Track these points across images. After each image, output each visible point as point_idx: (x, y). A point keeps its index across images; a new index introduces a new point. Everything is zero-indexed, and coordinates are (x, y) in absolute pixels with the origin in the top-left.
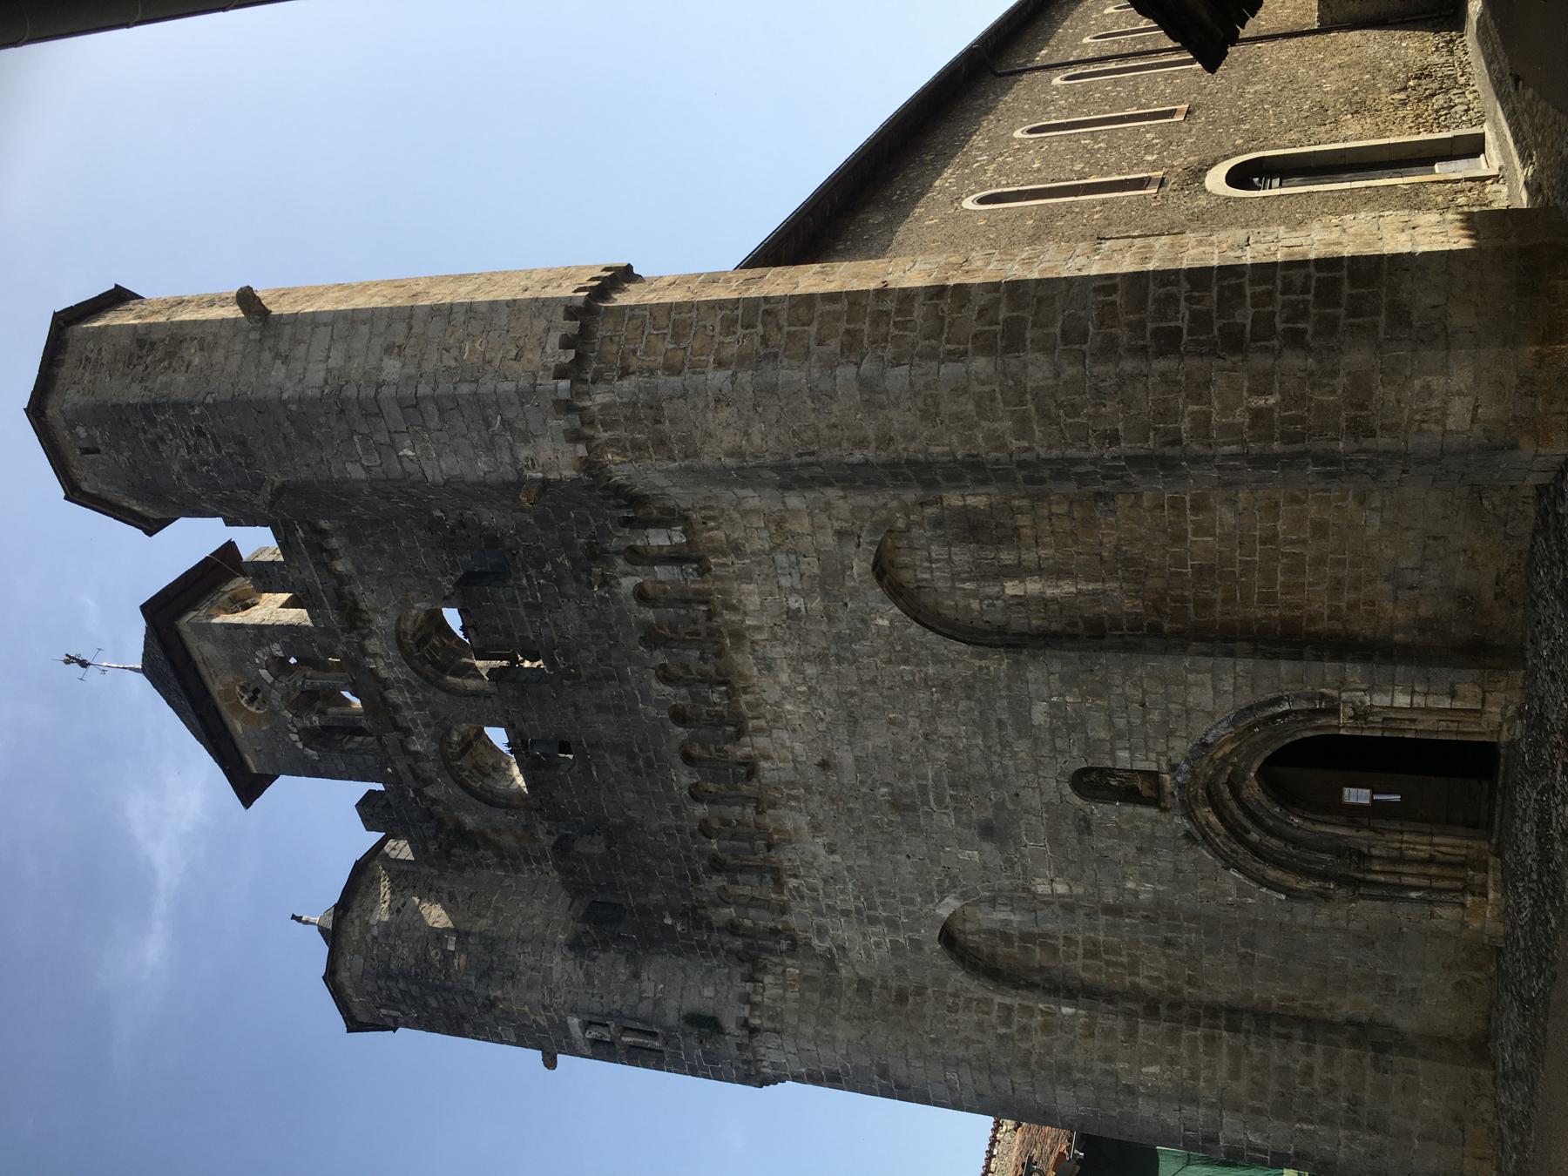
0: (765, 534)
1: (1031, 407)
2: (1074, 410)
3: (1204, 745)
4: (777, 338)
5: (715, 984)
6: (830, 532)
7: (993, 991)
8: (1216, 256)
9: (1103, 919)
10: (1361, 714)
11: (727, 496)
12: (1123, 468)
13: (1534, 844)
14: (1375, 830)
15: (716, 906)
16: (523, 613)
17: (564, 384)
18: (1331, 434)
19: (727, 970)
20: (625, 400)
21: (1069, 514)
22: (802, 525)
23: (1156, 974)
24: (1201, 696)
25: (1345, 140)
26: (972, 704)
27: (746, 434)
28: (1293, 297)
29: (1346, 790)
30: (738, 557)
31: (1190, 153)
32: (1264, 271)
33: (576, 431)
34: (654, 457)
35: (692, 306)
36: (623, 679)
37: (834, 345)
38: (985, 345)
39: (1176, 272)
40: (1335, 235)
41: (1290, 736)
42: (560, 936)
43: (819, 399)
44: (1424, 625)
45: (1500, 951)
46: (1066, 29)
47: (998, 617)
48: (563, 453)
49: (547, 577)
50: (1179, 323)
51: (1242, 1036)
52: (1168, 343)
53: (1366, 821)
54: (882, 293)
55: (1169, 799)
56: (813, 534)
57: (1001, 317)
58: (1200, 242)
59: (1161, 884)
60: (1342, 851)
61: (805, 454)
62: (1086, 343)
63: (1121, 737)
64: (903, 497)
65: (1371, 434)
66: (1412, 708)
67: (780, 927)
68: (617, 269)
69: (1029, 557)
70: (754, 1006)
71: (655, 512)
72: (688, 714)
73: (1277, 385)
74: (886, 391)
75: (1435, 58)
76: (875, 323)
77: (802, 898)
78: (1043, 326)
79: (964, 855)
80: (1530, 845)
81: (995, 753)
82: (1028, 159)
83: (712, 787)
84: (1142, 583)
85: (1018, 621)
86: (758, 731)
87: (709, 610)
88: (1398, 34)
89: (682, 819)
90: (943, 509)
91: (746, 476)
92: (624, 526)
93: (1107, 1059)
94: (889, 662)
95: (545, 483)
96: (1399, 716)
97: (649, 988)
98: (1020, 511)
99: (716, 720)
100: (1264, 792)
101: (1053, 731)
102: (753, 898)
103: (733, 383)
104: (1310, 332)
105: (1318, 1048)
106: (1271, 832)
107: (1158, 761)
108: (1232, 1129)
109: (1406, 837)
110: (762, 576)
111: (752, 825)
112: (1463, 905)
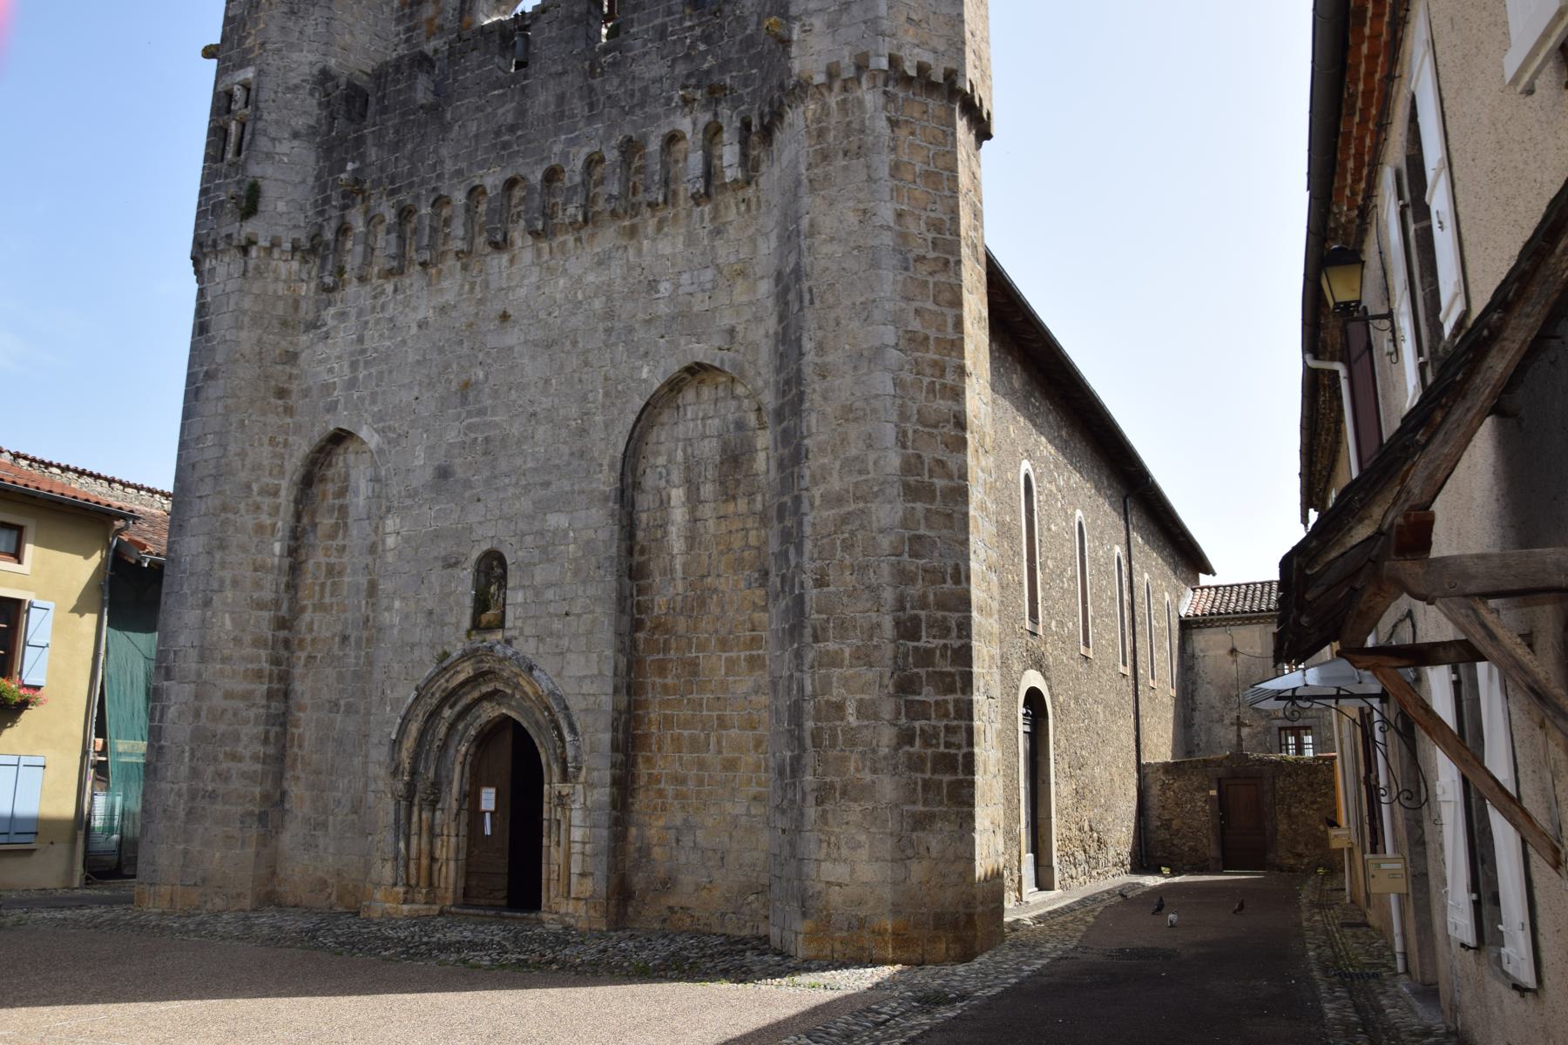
0: (732, 259)
1: (852, 507)
2: (848, 546)
3: (531, 669)
4: (923, 269)
5: (289, 213)
6: (733, 322)
7: (291, 479)
8: (980, 670)
9: (363, 581)
10: (562, 801)
11: (770, 222)
12: (792, 590)
13: (454, 939)
14: (458, 814)
15: (366, 212)
16: (658, 21)
17: (884, 63)
18: (820, 770)
19: (302, 224)
20: (867, 123)
21: (747, 546)
22: (740, 293)
23: (316, 627)
24: (577, 665)
25: (1056, 783)
26: (566, 458)
27: (832, 239)
28: (942, 735)
29: (493, 790)
30: (711, 232)
31: (1055, 659)
32: (966, 711)
33: (838, 75)
34: (811, 150)
35: (954, 191)
36: (590, 120)
37: (915, 324)
38: (911, 466)
39: (969, 636)
40: (992, 769)
41: (541, 743)
42: (333, 61)
43: (864, 309)
44: (645, 851)
45: (357, 914)
46: (1155, 559)
47: (649, 481)
48: (816, 60)
49: (693, 46)
50: (924, 639)
51: (264, 702)
52: (908, 629)
53: (466, 806)
54: (961, 371)
55: (479, 638)
56: (731, 305)
57: (935, 480)
58: (992, 657)
59: (400, 631)
60: (436, 786)
61: (811, 294)
62: (910, 556)
63: (537, 595)
64: (766, 392)
65: (819, 802)
66: (570, 842)
67: (346, 276)
68: (988, 125)
69: (707, 511)
70: (269, 251)
71: (755, 153)
72: (555, 184)
73: (866, 723)
74: (871, 372)
75: (1112, 853)
76: (935, 364)
77: (375, 297)
78: (926, 518)
79: (420, 452)
80: (453, 936)
81: (519, 479)
82: (1059, 520)
83: (483, 208)
84: (681, 613)
85: (645, 501)
86: (539, 253)
87: (657, 205)
88: (1132, 825)
89: (450, 179)
90: (754, 430)
91: (790, 237)
92: (743, 121)
93: (235, 583)
94: (606, 379)
95: (785, 42)
96: (562, 831)
97: (283, 147)
98: (751, 502)
99: (548, 211)
100: (488, 722)
101: (541, 533)
102: (373, 250)
103: (881, 226)
104: (911, 750)
105: (259, 767)
106: (452, 727)
107: (514, 628)
108: (179, 693)
109: (453, 839)
110: (691, 256)
111: (446, 248)
112: (395, 884)
